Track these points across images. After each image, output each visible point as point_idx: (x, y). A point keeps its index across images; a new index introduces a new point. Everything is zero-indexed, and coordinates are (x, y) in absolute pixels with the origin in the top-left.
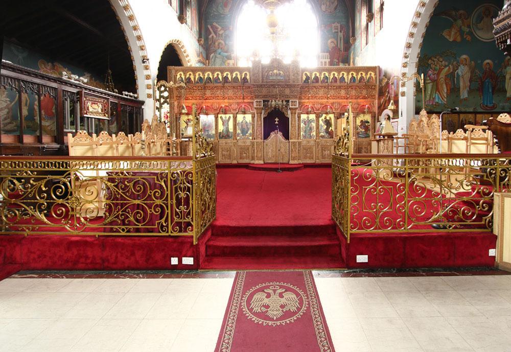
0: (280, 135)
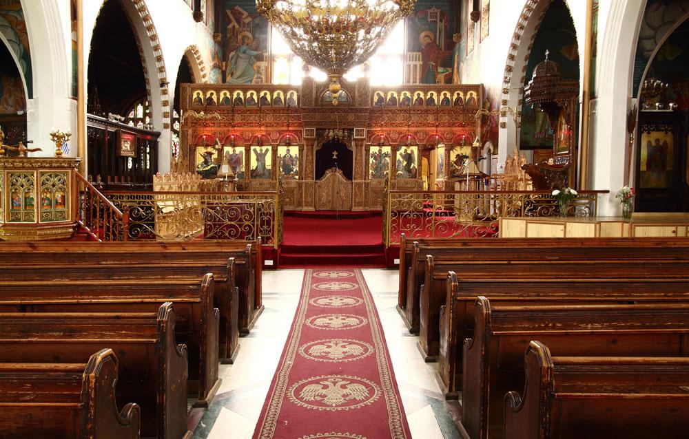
0: (339, 174)
